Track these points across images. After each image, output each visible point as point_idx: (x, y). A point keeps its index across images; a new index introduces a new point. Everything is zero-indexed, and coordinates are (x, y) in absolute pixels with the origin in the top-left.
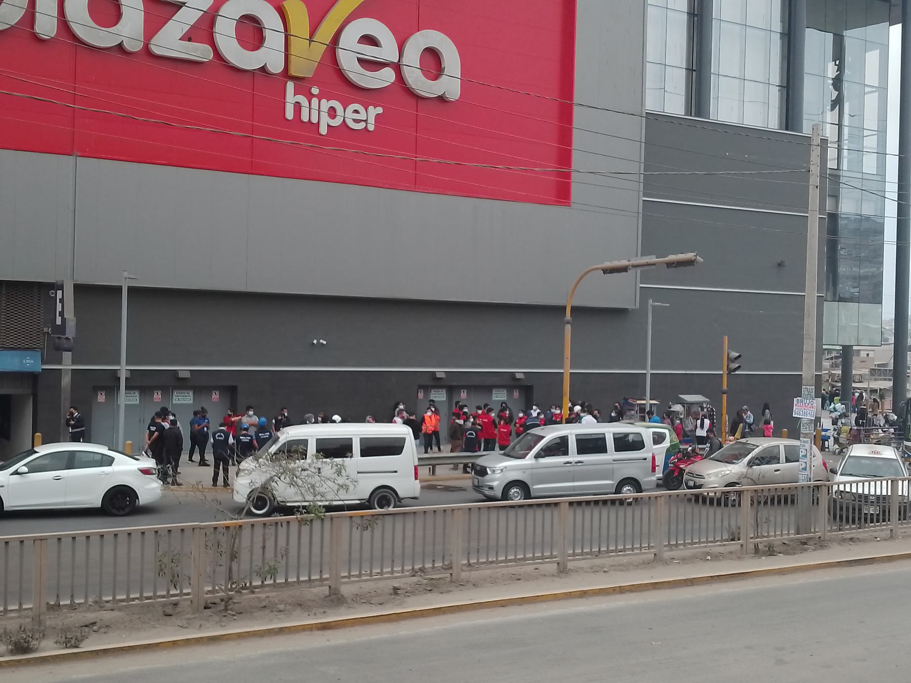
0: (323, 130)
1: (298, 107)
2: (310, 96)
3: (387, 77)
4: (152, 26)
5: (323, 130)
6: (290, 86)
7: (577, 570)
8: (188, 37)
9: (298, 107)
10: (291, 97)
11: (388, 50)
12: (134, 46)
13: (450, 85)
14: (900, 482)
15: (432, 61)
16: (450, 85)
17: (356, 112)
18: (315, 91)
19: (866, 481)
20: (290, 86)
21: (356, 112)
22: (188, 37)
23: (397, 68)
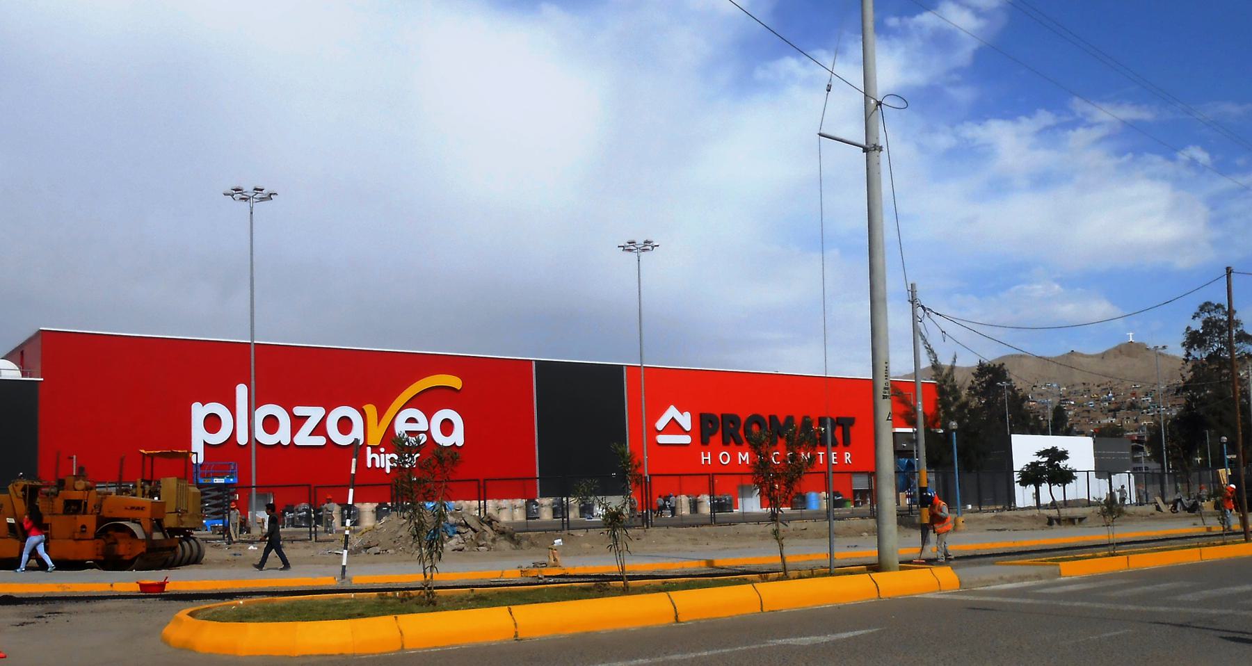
0: (388, 471)
1: (373, 459)
2: (379, 453)
3: (423, 438)
4: (294, 430)
5: (388, 471)
6: (369, 449)
7: (211, 564)
8: (305, 418)
9: (373, 459)
10: (370, 456)
11: (422, 425)
12: (286, 442)
13: (457, 437)
14: (1134, 501)
15: (447, 427)
16: (457, 437)
17: (412, 420)
18: (382, 450)
19: (1046, 507)
20: (369, 449)
21: (412, 420)
22: (305, 418)
23: (428, 433)
